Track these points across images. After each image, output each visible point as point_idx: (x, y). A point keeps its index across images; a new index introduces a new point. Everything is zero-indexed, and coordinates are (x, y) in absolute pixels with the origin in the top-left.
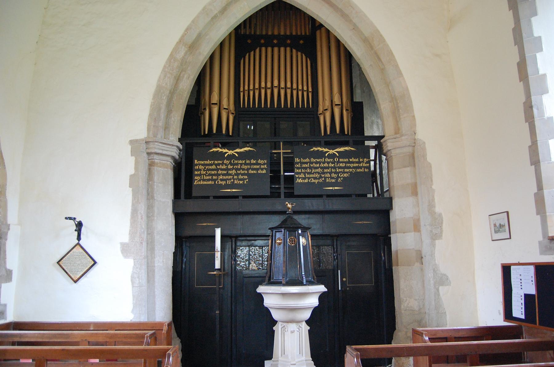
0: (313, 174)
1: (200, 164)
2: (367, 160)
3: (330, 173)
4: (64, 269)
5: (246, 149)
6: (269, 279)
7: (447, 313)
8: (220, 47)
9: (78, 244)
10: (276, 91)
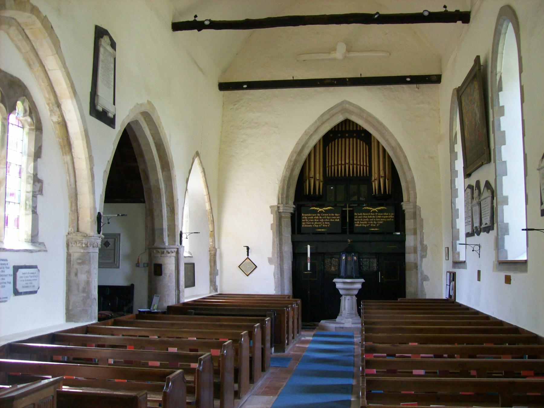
0: (364, 221)
1: (305, 216)
3: (373, 221)
4: (242, 270)
6: (339, 275)
7: (427, 295)
9: (248, 258)
10: (347, 166)
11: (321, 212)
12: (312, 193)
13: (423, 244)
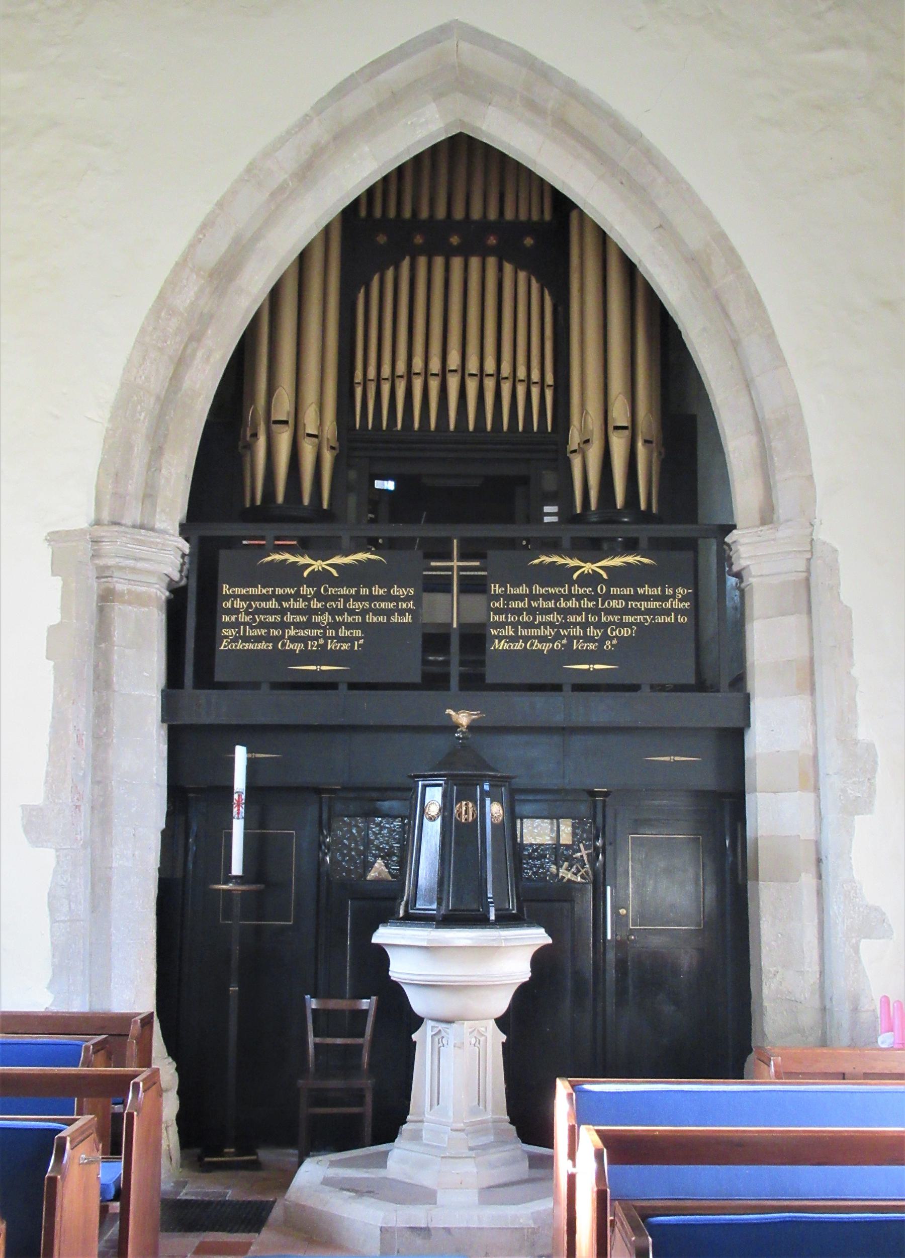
0: (538, 627)
1: (235, 597)
2: (684, 591)
3: (584, 626)
5: (361, 556)
8: (297, 266)
10: (453, 383)
11: (318, 578)
12: (280, 499)
13: (856, 742)
